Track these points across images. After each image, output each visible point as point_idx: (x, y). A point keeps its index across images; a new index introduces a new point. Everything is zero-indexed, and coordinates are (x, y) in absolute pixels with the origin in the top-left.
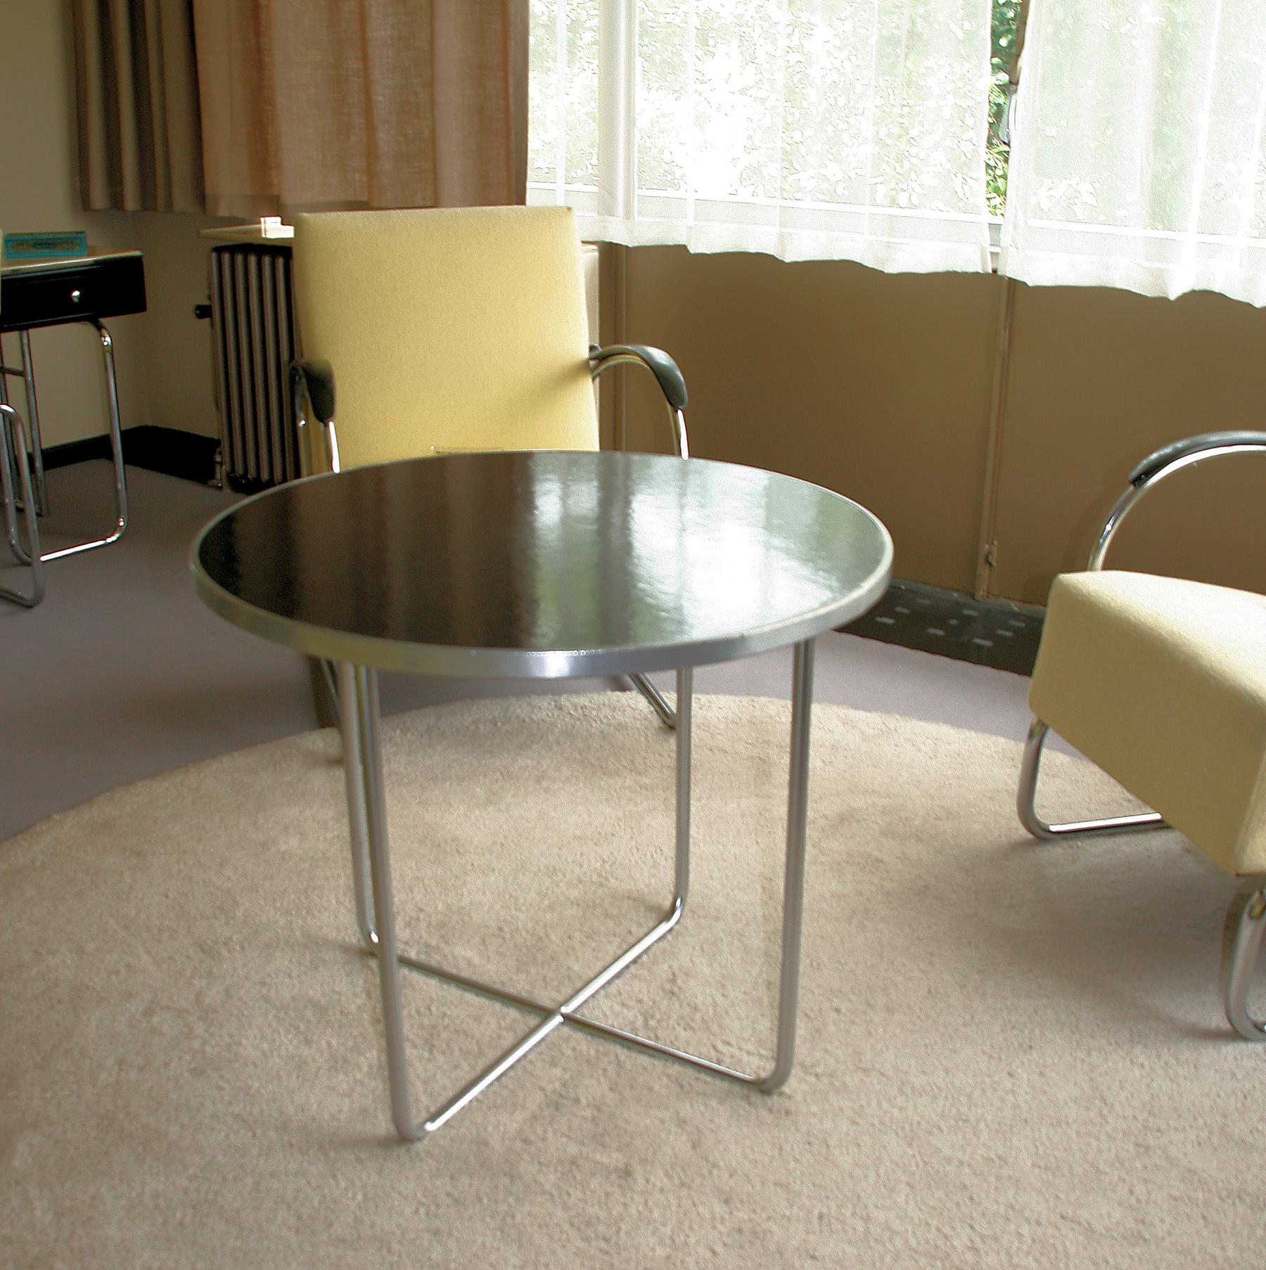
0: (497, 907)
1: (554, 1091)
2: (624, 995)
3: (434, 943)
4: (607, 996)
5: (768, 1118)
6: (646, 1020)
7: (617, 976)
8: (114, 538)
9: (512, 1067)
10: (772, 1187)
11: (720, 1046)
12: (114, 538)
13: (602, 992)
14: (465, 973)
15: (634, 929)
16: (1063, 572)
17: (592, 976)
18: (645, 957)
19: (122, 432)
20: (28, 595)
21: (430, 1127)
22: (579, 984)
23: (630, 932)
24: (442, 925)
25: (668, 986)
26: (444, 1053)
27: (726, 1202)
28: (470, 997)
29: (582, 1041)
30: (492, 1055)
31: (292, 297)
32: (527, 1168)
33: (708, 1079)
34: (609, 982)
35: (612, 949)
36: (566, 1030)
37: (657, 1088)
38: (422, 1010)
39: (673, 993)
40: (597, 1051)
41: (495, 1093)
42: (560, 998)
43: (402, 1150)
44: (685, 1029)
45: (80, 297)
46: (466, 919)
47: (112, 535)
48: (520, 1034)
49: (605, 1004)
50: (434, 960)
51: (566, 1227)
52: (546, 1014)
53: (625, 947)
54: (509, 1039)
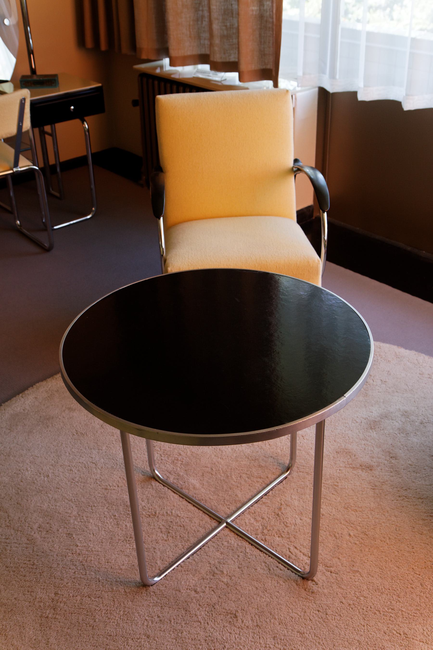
0: (213, 456)
1: (214, 565)
2: (257, 513)
3: (181, 474)
4: (249, 513)
5: (303, 593)
6: (263, 529)
7: (256, 502)
8: (89, 217)
9: (200, 548)
10: (296, 633)
11: (292, 548)
12: (89, 217)
13: (247, 511)
14: (191, 494)
15: (269, 476)
16: (160, 94)
17: (245, 500)
18: (271, 493)
19: (92, 154)
20: (47, 245)
21: (157, 579)
22: (239, 505)
23: (267, 477)
24: (187, 464)
25: (277, 511)
26: (173, 537)
27: (274, 638)
28: (190, 507)
29: (233, 540)
30: (193, 540)
31: (159, 141)
32: (193, 606)
33: (282, 567)
34: (252, 505)
35: (258, 486)
36: (227, 531)
37: (259, 569)
38: (169, 512)
39: (278, 515)
40: (238, 545)
41: (189, 562)
42: (229, 512)
43: (144, 591)
44: (279, 537)
45: (73, 109)
46: (198, 461)
47: (89, 215)
48: (208, 531)
49: (248, 518)
50: (180, 484)
51: (203, 641)
52: (220, 523)
53: (264, 485)
54: (202, 532)
